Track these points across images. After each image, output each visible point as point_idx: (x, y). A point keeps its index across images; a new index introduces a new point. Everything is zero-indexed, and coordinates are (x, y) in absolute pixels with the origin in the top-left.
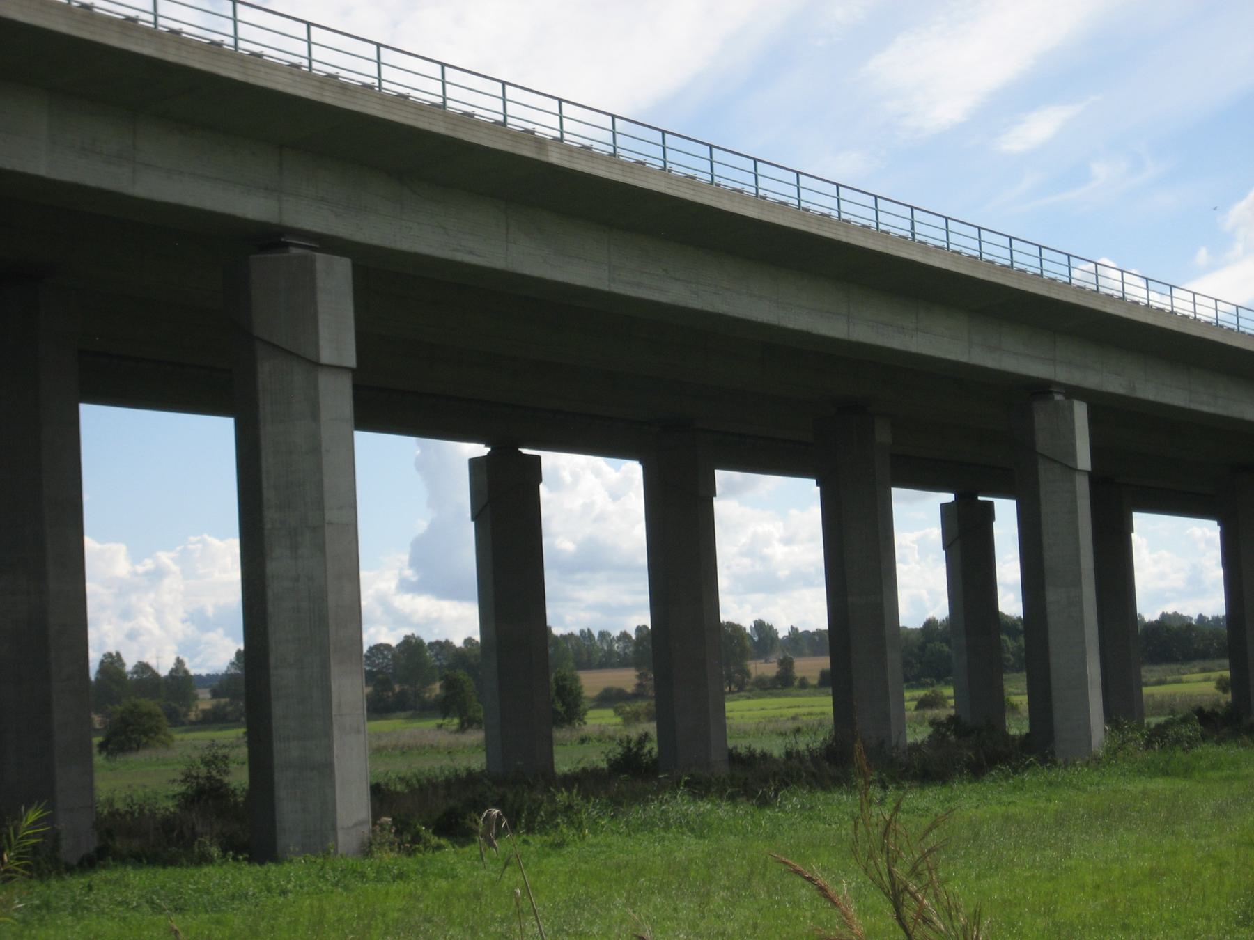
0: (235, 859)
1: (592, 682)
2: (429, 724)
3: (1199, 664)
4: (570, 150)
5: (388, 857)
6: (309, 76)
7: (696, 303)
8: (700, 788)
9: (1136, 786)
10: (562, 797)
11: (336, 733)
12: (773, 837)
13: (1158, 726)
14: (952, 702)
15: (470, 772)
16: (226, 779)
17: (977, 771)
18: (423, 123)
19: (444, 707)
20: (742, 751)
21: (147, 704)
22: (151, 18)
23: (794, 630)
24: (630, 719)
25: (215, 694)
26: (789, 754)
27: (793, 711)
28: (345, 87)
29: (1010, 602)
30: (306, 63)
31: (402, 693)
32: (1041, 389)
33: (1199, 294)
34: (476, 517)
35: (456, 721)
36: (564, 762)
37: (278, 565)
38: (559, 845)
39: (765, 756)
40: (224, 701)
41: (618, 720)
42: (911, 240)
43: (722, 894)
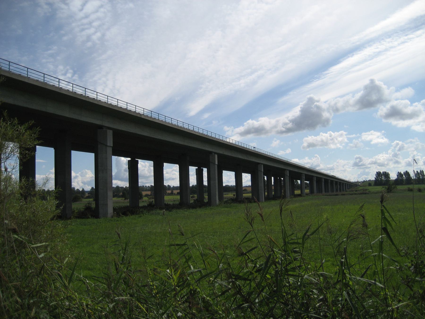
0: (93, 218)
1: (144, 193)
2: (120, 199)
3: (231, 192)
4: (145, 116)
5: (116, 218)
6: (107, 104)
7: (162, 139)
8: (161, 209)
9: (223, 209)
10: (141, 210)
11: (108, 200)
12: (171, 216)
13: (226, 201)
14: (196, 197)
15: (127, 206)
16: (91, 206)
17: (200, 207)
18: (124, 111)
19: (122, 196)
20: (166, 203)
21: (78, 195)
22: (96, 98)
23: (173, 186)
24: (150, 199)
25: (88, 194)
26: (173, 204)
27: (173, 198)
28: (113, 106)
29: (205, 183)
30: (107, 102)
31: (116, 194)
32: (211, 153)
33: (12, 62)
34: (196, 175)
35: (124, 198)
36: (141, 205)
37: (100, 175)
38: (141, 217)
39: (170, 204)
40: (90, 195)
41: (148, 199)
42: (193, 131)
43: (165, 224)
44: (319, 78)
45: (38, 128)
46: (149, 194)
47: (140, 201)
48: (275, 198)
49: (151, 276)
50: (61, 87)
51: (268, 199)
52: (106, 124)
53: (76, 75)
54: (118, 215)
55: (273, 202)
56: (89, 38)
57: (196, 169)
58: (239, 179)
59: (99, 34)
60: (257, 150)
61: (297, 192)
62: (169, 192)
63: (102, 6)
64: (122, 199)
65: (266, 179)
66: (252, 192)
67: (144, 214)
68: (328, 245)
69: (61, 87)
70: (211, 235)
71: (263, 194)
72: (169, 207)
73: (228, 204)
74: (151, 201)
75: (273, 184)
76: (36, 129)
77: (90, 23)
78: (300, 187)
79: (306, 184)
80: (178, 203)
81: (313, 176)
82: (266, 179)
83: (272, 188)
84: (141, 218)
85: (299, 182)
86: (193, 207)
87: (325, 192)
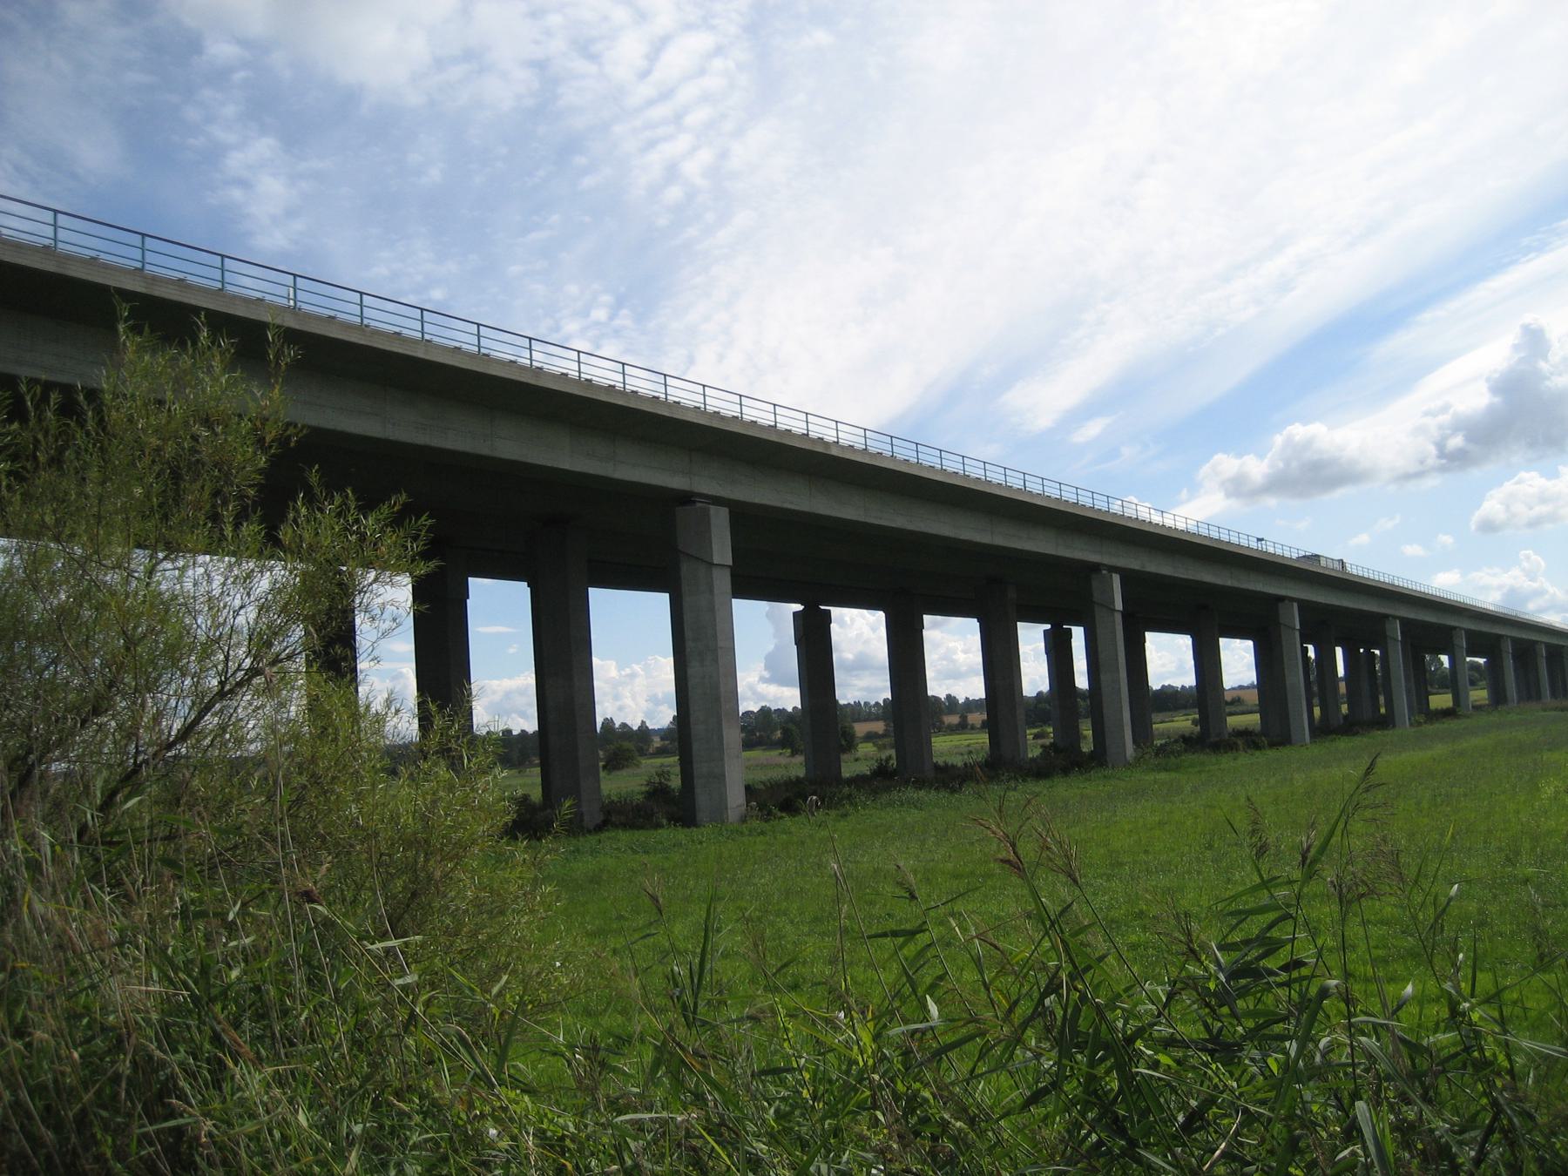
1: (860, 729)
3: (1184, 712)
5: (756, 823)
8: (921, 784)
9: (1150, 777)
11: (726, 759)
16: (669, 784)
17: (1065, 771)
18: (765, 436)
19: (782, 744)
21: (627, 745)
24: (881, 748)
25: (662, 739)
28: (723, 418)
29: (1082, 681)
30: (703, 406)
31: (761, 736)
32: (1095, 568)
35: (789, 751)
36: (849, 769)
37: (694, 670)
40: (667, 742)
41: (875, 749)
42: (1024, 491)
44: (1541, 248)
45: (424, 518)
46: (881, 732)
47: (844, 757)
48: (1350, 727)
49: (790, 1035)
50: (539, 365)
51: (1322, 731)
52: (705, 484)
53: (624, 312)
54: (767, 816)
55: (1343, 743)
56: (672, 172)
57: (1045, 631)
58: (1207, 662)
59: (705, 156)
60: (1271, 550)
61: (1442, 700)
62: (954, 720)
63: (719, 51)
64: (781, 754)
65: (1311, 654)
66: (991, 726)
67: (856, 806)
68: (1555, 907)
69: (538, 368)
70: (1101, 876)
71: (1304, 713)
72: (950, 778)
73: (1169, 757)
74: (884, 757)
75: (1341, 672)
76: (416, 522)
77: (678, 118)
78: (1450, 682)
79: (1475, 666)
80: (980, 757)
81: (1499, 637)
82: (1311, 654)
83: (1336, 688)
84: (849, 818)
85: (1445, 659)
86: (1040, 771)
87: (1554, 695)
